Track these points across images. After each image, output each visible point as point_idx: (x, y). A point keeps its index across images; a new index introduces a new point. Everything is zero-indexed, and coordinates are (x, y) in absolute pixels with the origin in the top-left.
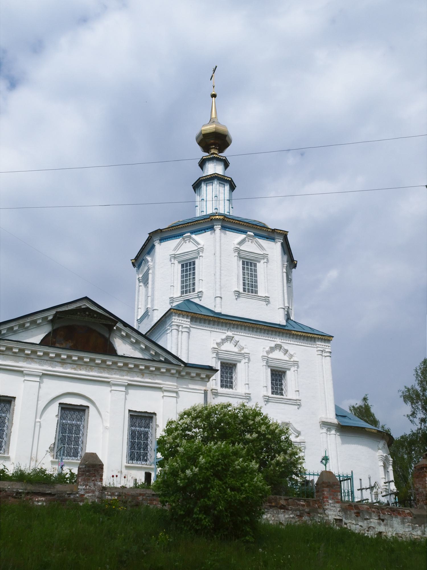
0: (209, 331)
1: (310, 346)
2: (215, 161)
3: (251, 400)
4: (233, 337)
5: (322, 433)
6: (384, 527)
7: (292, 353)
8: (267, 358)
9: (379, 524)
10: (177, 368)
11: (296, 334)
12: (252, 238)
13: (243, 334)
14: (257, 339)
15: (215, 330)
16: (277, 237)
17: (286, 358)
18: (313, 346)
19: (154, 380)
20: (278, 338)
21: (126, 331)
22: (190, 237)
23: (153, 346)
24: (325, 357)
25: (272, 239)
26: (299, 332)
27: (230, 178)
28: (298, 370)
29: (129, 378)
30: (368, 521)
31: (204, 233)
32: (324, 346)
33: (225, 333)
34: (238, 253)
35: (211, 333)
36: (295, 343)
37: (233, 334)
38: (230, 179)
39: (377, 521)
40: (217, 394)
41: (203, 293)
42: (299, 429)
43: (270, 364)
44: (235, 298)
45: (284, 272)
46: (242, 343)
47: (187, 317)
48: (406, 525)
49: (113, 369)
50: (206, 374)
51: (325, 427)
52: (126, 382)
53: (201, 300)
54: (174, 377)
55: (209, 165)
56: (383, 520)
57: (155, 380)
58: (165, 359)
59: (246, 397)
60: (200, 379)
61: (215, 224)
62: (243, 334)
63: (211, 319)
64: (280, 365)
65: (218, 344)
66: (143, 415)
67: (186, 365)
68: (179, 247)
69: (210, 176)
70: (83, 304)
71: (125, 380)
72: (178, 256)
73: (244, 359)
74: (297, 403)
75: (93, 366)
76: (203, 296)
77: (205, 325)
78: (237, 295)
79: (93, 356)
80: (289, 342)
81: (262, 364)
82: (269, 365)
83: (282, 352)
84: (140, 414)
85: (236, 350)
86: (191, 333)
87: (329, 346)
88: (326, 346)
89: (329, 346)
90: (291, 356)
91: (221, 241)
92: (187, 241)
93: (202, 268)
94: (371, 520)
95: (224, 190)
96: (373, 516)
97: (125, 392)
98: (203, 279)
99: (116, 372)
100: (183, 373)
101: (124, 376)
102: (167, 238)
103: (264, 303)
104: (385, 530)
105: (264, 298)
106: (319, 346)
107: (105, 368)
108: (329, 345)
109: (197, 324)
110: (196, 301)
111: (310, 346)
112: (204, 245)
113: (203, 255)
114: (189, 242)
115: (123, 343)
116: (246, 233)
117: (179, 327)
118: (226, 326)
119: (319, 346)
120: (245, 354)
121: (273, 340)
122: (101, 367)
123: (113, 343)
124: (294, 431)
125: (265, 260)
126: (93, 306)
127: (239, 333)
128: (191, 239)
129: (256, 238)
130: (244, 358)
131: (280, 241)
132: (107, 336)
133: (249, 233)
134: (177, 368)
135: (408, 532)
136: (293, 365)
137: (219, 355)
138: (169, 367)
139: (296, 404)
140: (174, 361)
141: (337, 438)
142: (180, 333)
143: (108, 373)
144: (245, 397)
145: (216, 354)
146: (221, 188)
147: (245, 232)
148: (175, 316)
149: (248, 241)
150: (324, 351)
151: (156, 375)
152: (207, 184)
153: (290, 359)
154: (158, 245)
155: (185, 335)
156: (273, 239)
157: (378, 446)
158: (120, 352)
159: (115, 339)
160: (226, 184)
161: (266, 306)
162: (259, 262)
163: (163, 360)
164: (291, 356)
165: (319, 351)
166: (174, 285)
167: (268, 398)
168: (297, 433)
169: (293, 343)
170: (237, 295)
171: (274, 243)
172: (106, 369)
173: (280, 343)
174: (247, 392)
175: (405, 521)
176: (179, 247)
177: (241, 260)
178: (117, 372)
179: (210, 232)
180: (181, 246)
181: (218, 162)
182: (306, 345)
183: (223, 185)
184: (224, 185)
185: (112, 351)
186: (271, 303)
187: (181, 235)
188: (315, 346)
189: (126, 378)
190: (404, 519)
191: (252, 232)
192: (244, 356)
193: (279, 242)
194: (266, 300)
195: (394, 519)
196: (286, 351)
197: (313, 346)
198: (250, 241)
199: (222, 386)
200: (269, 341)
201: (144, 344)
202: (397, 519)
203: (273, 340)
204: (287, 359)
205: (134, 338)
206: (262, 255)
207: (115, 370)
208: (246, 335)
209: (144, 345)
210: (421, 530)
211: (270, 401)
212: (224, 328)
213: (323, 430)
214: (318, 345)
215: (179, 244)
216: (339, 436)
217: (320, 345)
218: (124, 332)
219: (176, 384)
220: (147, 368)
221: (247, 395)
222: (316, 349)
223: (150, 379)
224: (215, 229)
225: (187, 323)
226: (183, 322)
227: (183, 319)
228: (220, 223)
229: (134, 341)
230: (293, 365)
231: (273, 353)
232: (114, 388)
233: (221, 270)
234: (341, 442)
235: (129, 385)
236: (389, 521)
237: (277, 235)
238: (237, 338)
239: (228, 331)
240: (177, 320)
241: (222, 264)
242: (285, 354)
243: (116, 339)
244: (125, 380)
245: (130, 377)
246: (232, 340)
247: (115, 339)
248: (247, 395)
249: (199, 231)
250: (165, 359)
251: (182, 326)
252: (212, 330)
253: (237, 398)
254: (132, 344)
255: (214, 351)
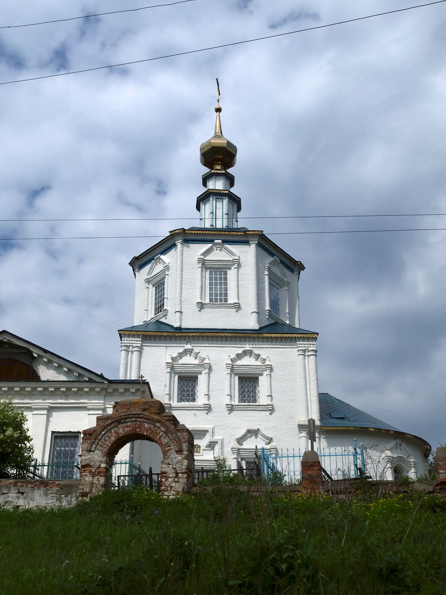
0: (165, 347)
1: (290, 347)
2: (214, 177)
3: (212, 410)
4: (192, 350)
5: (300, 437)
6: (23, 500)
7: (264, 357)
8: (231, 366)
9: (18, 498)
10: (102, 386)
11: (289, 337)
12: (220, 246)
13: (205, 345)
14: (222, 348)
15: (172, 345)
16: (250, 239)
17: (258, 363)
18: (293, 347)
19: (78, 400)
20: (248, 344)
21: (47, 357)
22: (159, 258)
23: (75, 368)
24: (309, 356)
25: (246, 243)
26: (139, 331)
27: (227, 190)
28: (272, 374)
29: (51, 401)
30: (5, 495)
31: (170, 251)
32: (308, 344)
33: (184, 347)
34: (202, 264)
35: (167, 348)
36: (270, 346)
37: (192, 346)
38: (227, 192)
39: (15, 495)
40: (171, 408)
41: (168, 310)
42: (270, 436)
43: (236, 372)
44: (198, 309)
45: (266, 275)
46: (202, 355)
47: (138, 336)
48: (50, 496)
49: (35, 395)
50: (135, 388)
51: (303, 430)
52: (47, 406)
53: (166, 318)
54: (101, 395)
55: (209, 183)
56: (22, 493)
57: (80, 400)
58: (90, 379)
59: (204, 407)
60: (131, 394)
61: (250, 239)
62: (205, 345)
63: (255, 336)
64: (250, 372)
65: (173, 359)
66: (67, 434)
67: (110, 382)
68: (152, 270)
69: (205, 194)
70: (4, 337)
71: (47, 403)
72: (152, 280)
73: (204, 370)
74: (271, 409)
75: (14, 394)
76: (169, 314)
77: (160, 342)
78: (200, 306)
79: (11, 384)
80: (263, 346)
81: (226, 373)
82: (235, 372)
83: (254, 358)
84: (64, 435)
85: (197, 362)
86: (144, 353)
87: (313, 345)
88: (310, 345)
89: (313, 345)
90: (264, 360)
91: (183, 255)
92: (158, 263)
93: (168, 286)
94: (10, 494)
95: (223, 204)
96: (12, 490)
97: (46, 415)
98: (168, 297)
99: (38, 397)
100: (110, 390)
101: (46, 400)
102: (147, 263)
103: (234, 310)
104: (24, 504)
105: (233, 305)
106: (300, 345)
107: (27, 394)
108: (314, 343)
109: (147, 341)
110: (163, 320)
111: (290, 347)
112: (169, 263)
113: (169, 273)
114: (160, 263)
115: (47, 369)
116: (214, 242)
117: (129, 347)
118: (185, 340)
119: (300, 345)
120: (204, 365)
121: (243, 346)
122: (22, 394)
123: (36, 370)
124: (264, 438)
125: (236, 266)
126: (12, 338)
127: (206, 344)
128: (160, 260)
129: (225, 245)
130: (205, 369)
131: (254, 242)
132: (29, 363)
133: (216, 241)
134: (101, 386)
135: (51, 503)
136: (265, 369)
137: (176, 370)
138: (92, 385)
139: (268, 409)
140: (98, 379)
141: (321, 441)
142: (307, 357)
143: (30, 399)
144: (204, 409)
145: (208, 369)
146: (219, 203)
147: (212, 241)
148: (125, 337)
149: (217, 250)
150: (307, 350)
151: (81, 395)
152: (205, 202)
153: (264, 363)
154: (138, 273)
155: (312, 358)
156: (246, 242)
157: (386, 447)
158: (43, 378)
159: (39, 366)
160: (224, 198)
161: (236, 312)
162: (230, 269)
163: (87, 379)
164: (264, 360)
165: (300, 351)
166: (148, 309)
167: (231, 406)
168: (268, 440)
169: (267, 346)
170: (200, 306)
171: (249, 246)
172: (28, 396)
173: (250, 349)
174: (207, 402)
175: (48, 492)
176: (152, 270)
177: (208, 271)
178: (39, 397)
179: (174, 249)
180: (153, 269)
181: (218, 177)
182: (284, 347)
183: (222, 200)
184: (223, 199)
185: (35, 377)
186: (242, 309)
187: (153, 259)
188: (296, 346)
189: (49, 402)
190: (48, 490)
191: (220, 240)
192: (204, 367)
193: (254, 243)
194: (237, 307)
195: (36, 491)
196: (258, 356)
197: (293, 347)
198: (219, 249)
199: (180, 400)
200: (236, 348)
201: (66, 367)
202: (39, 491)
203: (243, 346)
204: (260, 364)
205: (56, 363)
206: (232, 261)
207: (37, 396)
208: (217, 346)
209: (66, 368)
210: (67, 500)
211: (234, 409)
212: (183, 342)
213: (302, 434)
214: (299, 344)
215: (151, 268)
216: (324, 439)
217: (302, 345)
218: (46, 359)
219: (103, 402)
220: (69, 389)
221: (205, 406)
222: (296, 349)
223: (74, 400)
224: (177, 244)
225: (138, 342)
226: (133, 342)
227: (303, 343)
228: (181, 237)
229: (57, 365)
230: (265, 369)
231: (242, 359)
232: (35, 412)
233: (182, 285)
234: (327, 445)
235: (51, 408)
236: (29, 494)
237: (249, 237)
238: (196, 350)
239: (187, 345)
240: (127, 340)
241: (183, 278)
242: (257, 360)
243: (40, 366)
244: (47, 403)
245: (53, 400)
246: (191, 352)
247: (39, 366)
248: (205, 406)
249: (167, 250)
250: (90, 379)
251: (132, 346)
252: (167, 345)
253: (195, 410)
254: (56, 369)
255: (167, 366)
